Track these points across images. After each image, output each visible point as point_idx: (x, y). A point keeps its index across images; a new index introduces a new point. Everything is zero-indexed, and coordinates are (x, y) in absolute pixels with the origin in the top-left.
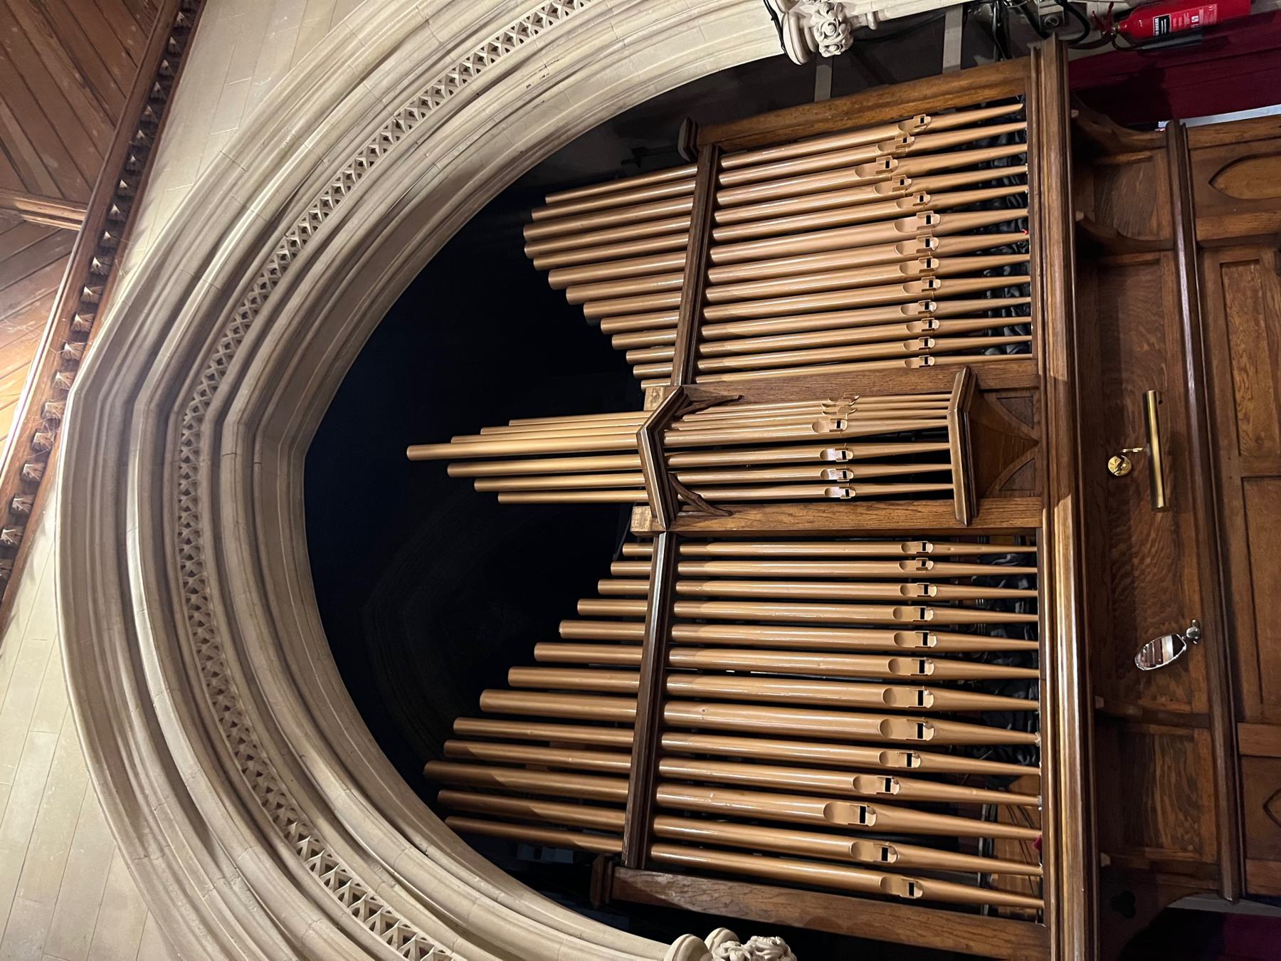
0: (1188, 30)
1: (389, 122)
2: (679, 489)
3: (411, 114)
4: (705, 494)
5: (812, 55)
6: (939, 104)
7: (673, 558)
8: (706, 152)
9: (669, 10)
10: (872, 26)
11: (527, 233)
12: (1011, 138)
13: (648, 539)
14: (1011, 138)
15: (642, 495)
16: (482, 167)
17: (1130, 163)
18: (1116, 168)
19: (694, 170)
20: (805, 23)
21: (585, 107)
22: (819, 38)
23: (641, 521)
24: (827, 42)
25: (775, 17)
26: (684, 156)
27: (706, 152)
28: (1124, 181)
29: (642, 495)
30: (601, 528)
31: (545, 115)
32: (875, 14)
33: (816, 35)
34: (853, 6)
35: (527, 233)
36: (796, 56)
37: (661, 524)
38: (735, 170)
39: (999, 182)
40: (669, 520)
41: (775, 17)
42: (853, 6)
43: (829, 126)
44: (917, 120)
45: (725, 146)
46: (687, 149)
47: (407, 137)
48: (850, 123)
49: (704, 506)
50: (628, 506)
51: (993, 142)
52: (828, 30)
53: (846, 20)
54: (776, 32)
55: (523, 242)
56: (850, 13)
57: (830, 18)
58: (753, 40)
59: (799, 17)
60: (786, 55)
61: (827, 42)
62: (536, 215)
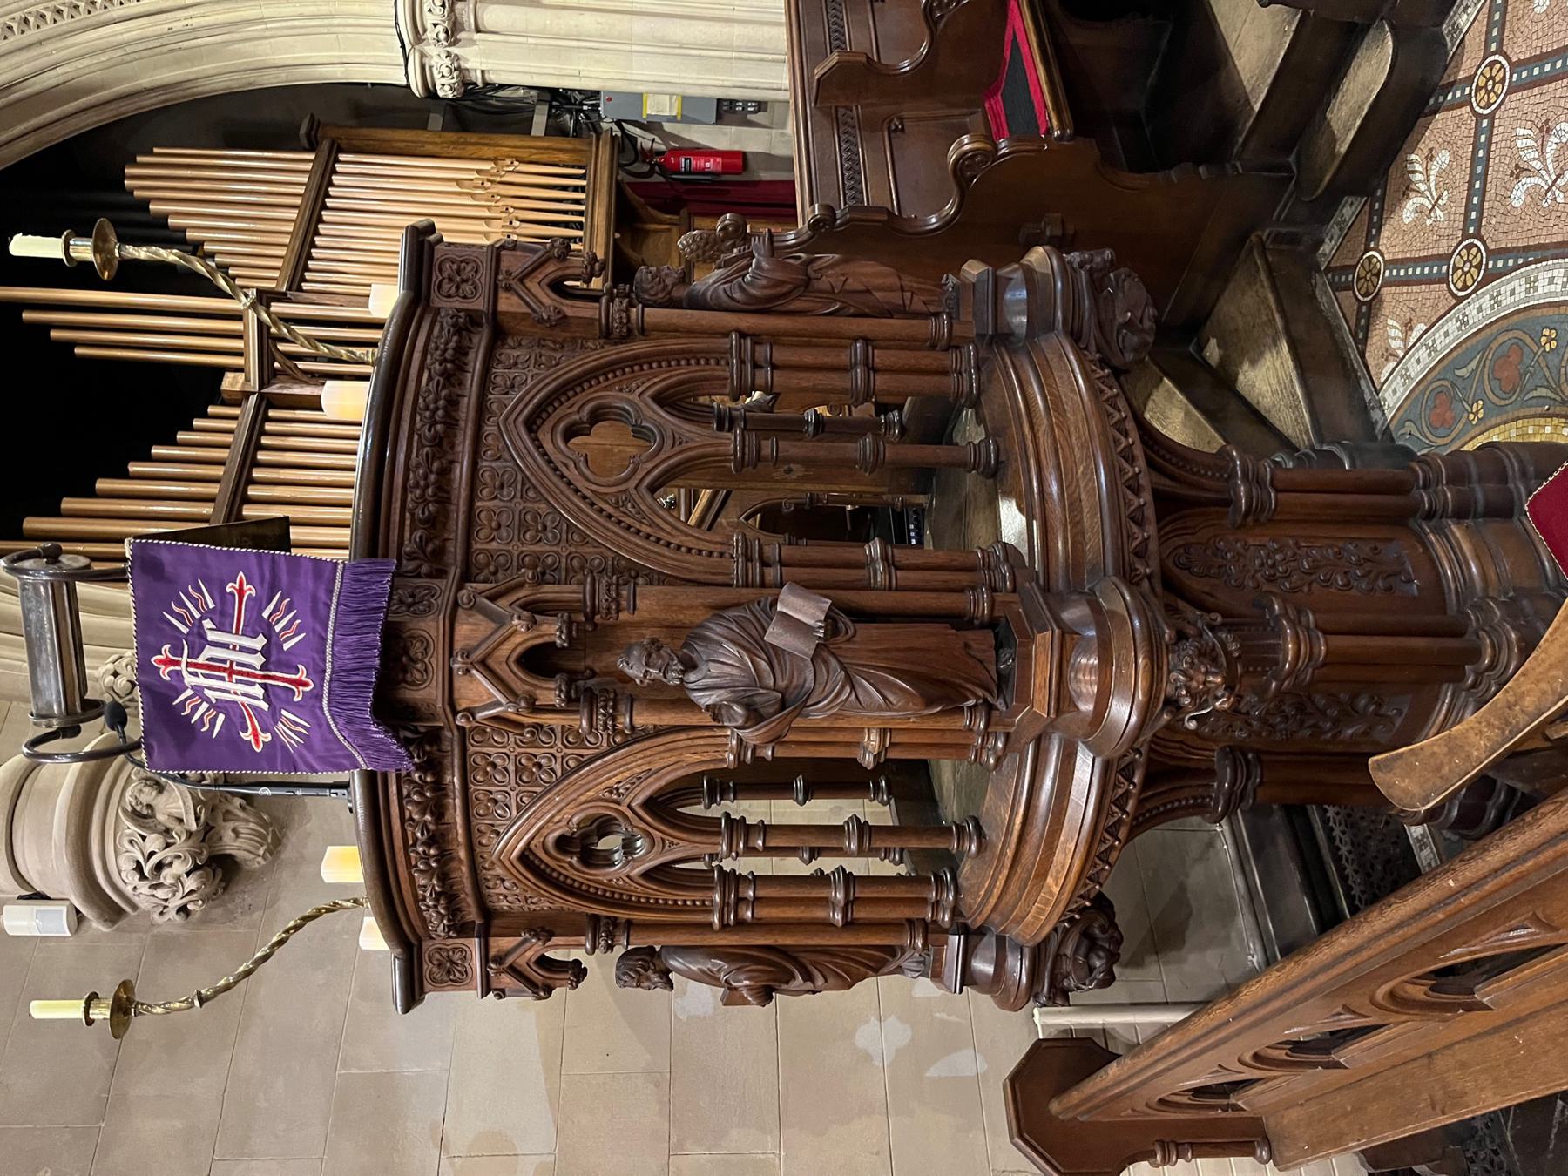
0: (703, 172)
1: (17, 15)
2: (278, 356)
3: (43, 16)
4: (301, 365)
5: (431, 93)
6: (524, 154)
7: (260, 418)
8: (325, 145)
9: (312, 9)
10: (480, 83)
11: (128, 171)
12: (576, 189)
13: (238, 400)
14: (576, 189)
15: (239, 361)
16: (102, 88)
17: (656, 231)
18: (647, 233)
19: (312, 156)
20: (426, 61)
21: (217, 71)
22: (437, 76)
23: (231, 383)
24: (443, 81)
25: (403, 47)
26: (304, 142)
27: (325, 145)
28: (651, 242)
29: (239, 361)
30: (192, 390)
31: (178, 63)
32: (483, 72)
33: (435, 72)
34: (467, 60)
35: (128, 171)
36: (417, 89)
37: (254, 385)
38: (347, 163)
39: (565, 212)
40: (262, 385)
41: (403, 47)
42: (467, 60)
43: (436, 149)
44: (508, 162)
45: (343, 143)
46: (308, 135)
47: (32, 34)
48: (456, 153)
49: (300, 375)
50: (220, 371)
51: (564, 188)
52: (446, 71)
53: (459, 69)
54: (402, 61)
55: (124, 176)
56: (464, 65)
57: (448, 62)
58: (378, 62)
59: (422, 56)
60: (408, 86)
61: (443, 81)
62: (139, 159)
